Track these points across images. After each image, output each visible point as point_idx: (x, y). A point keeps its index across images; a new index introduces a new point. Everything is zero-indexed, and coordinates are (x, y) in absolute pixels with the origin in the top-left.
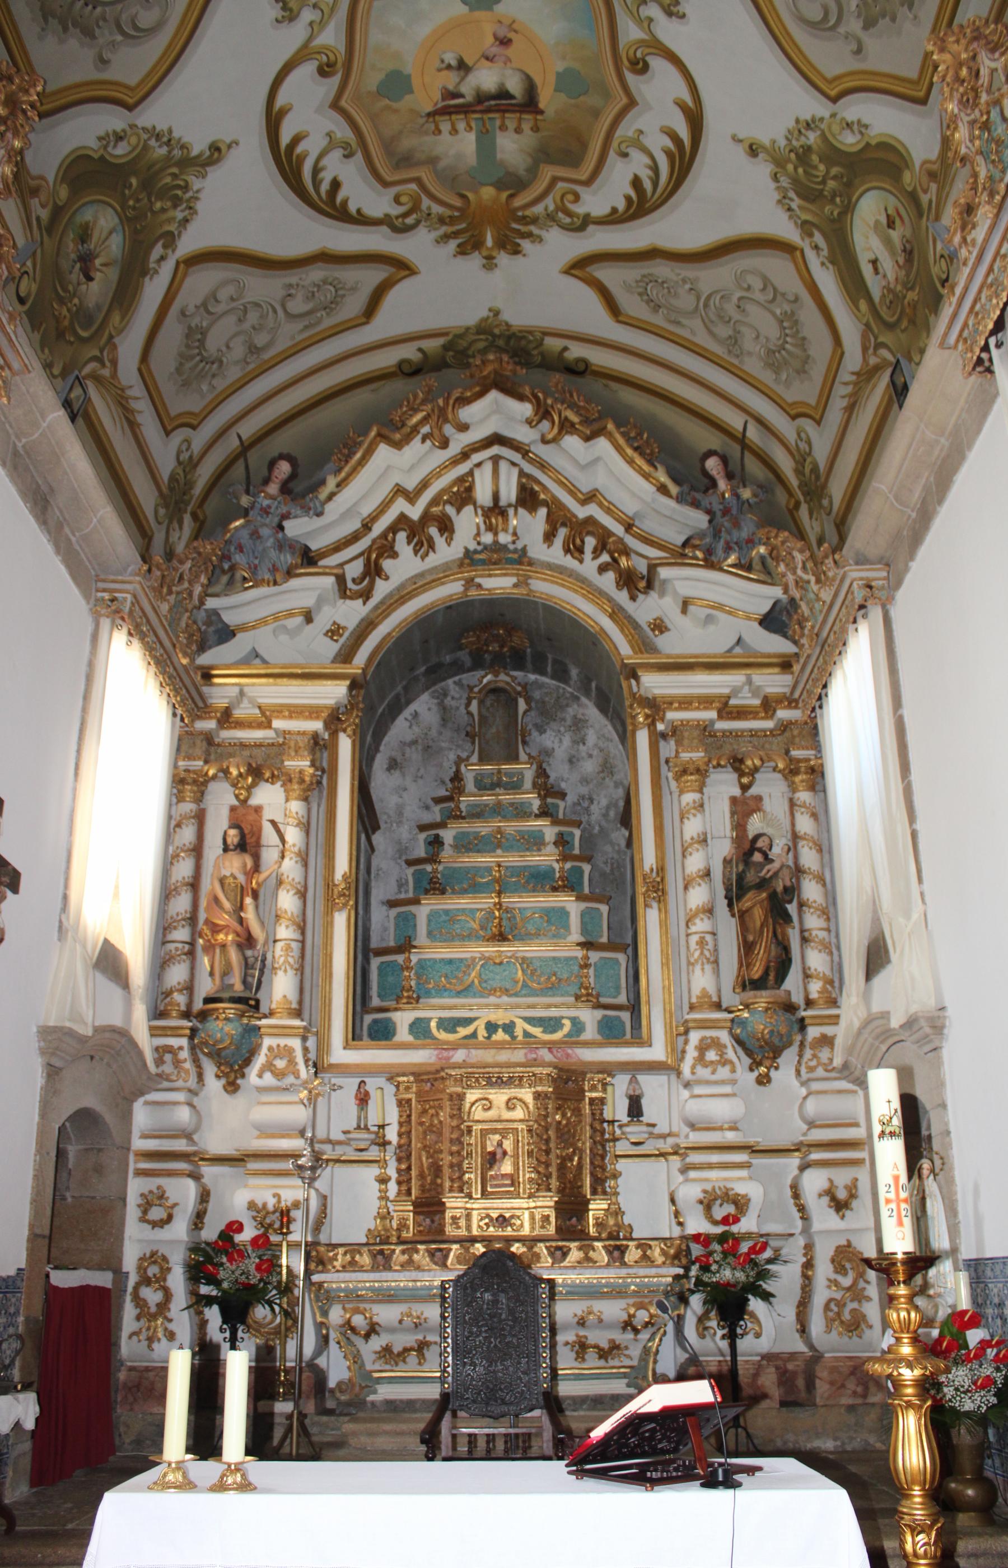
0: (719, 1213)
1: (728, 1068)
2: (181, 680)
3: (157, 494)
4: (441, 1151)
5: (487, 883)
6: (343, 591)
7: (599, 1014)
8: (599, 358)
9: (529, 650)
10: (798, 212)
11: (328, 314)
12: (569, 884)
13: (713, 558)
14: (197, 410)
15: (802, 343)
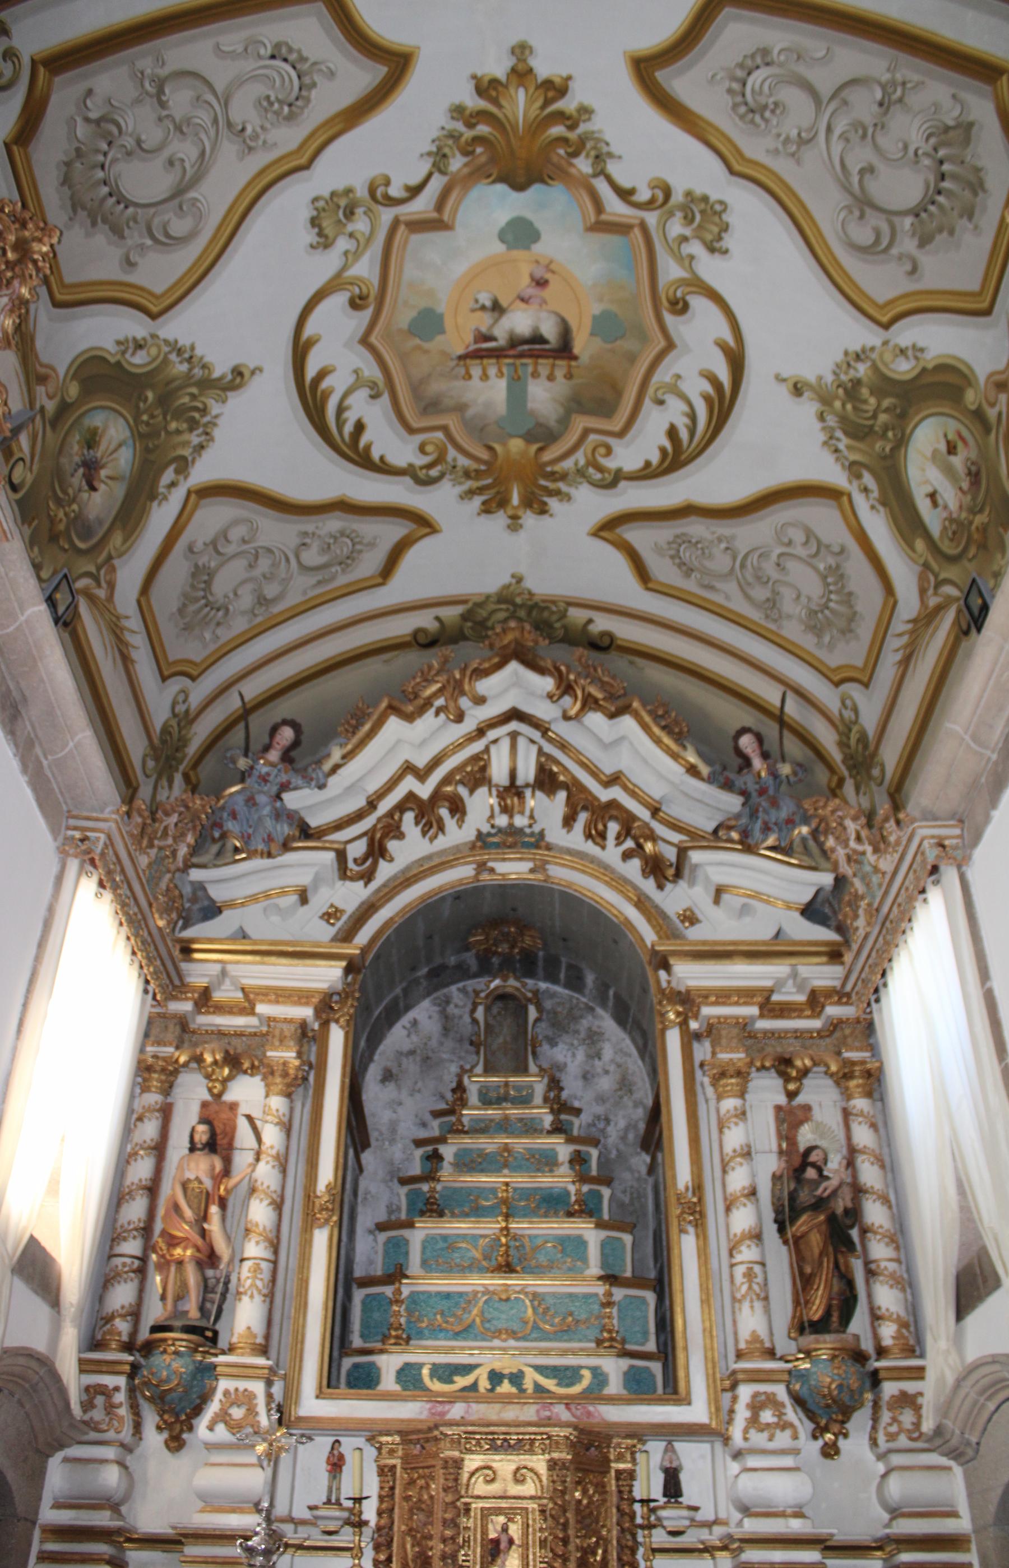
1: (788, 1433)
2: (156, 949)
3: (146, 742)
4: (430, 1537)
5: (491, 1207)
6: (343, 873)
7: (625, 1363)
8: (626, 631)
9: (541, 954)
10: (845, 452)
11: (343, 571)
12: (587, 1209)
13: (750, 841)
14: (198, 659)
15: (848, 598)
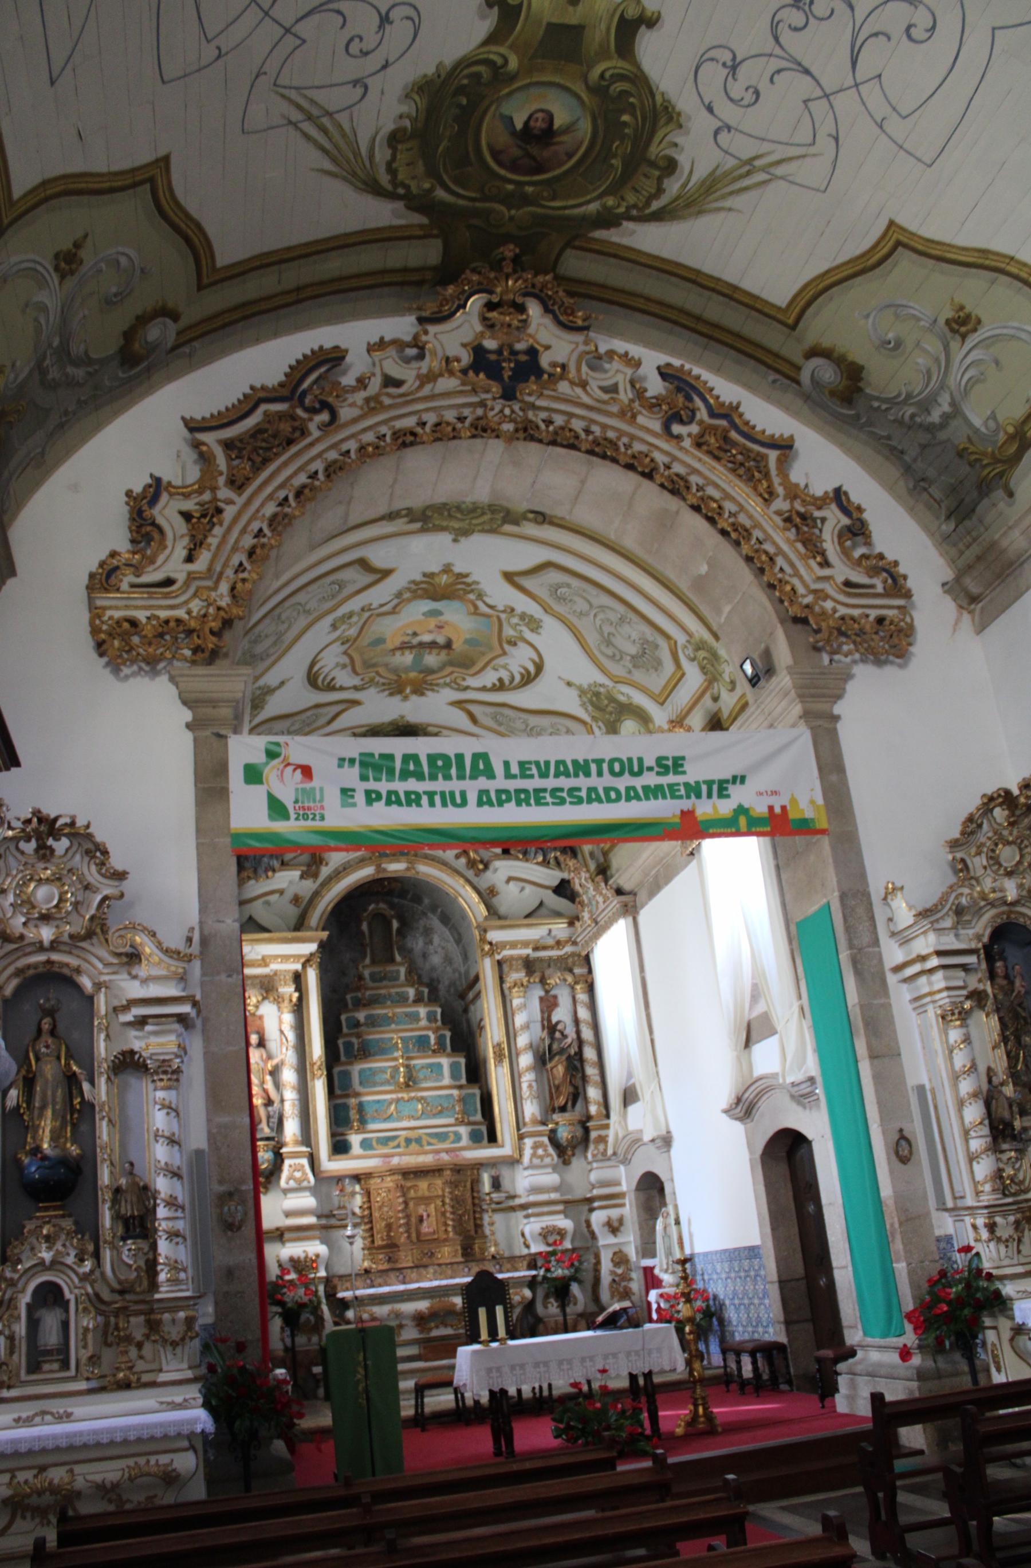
0: (551, 1240)
